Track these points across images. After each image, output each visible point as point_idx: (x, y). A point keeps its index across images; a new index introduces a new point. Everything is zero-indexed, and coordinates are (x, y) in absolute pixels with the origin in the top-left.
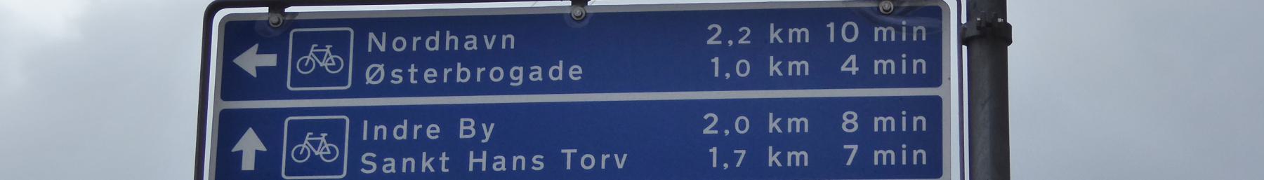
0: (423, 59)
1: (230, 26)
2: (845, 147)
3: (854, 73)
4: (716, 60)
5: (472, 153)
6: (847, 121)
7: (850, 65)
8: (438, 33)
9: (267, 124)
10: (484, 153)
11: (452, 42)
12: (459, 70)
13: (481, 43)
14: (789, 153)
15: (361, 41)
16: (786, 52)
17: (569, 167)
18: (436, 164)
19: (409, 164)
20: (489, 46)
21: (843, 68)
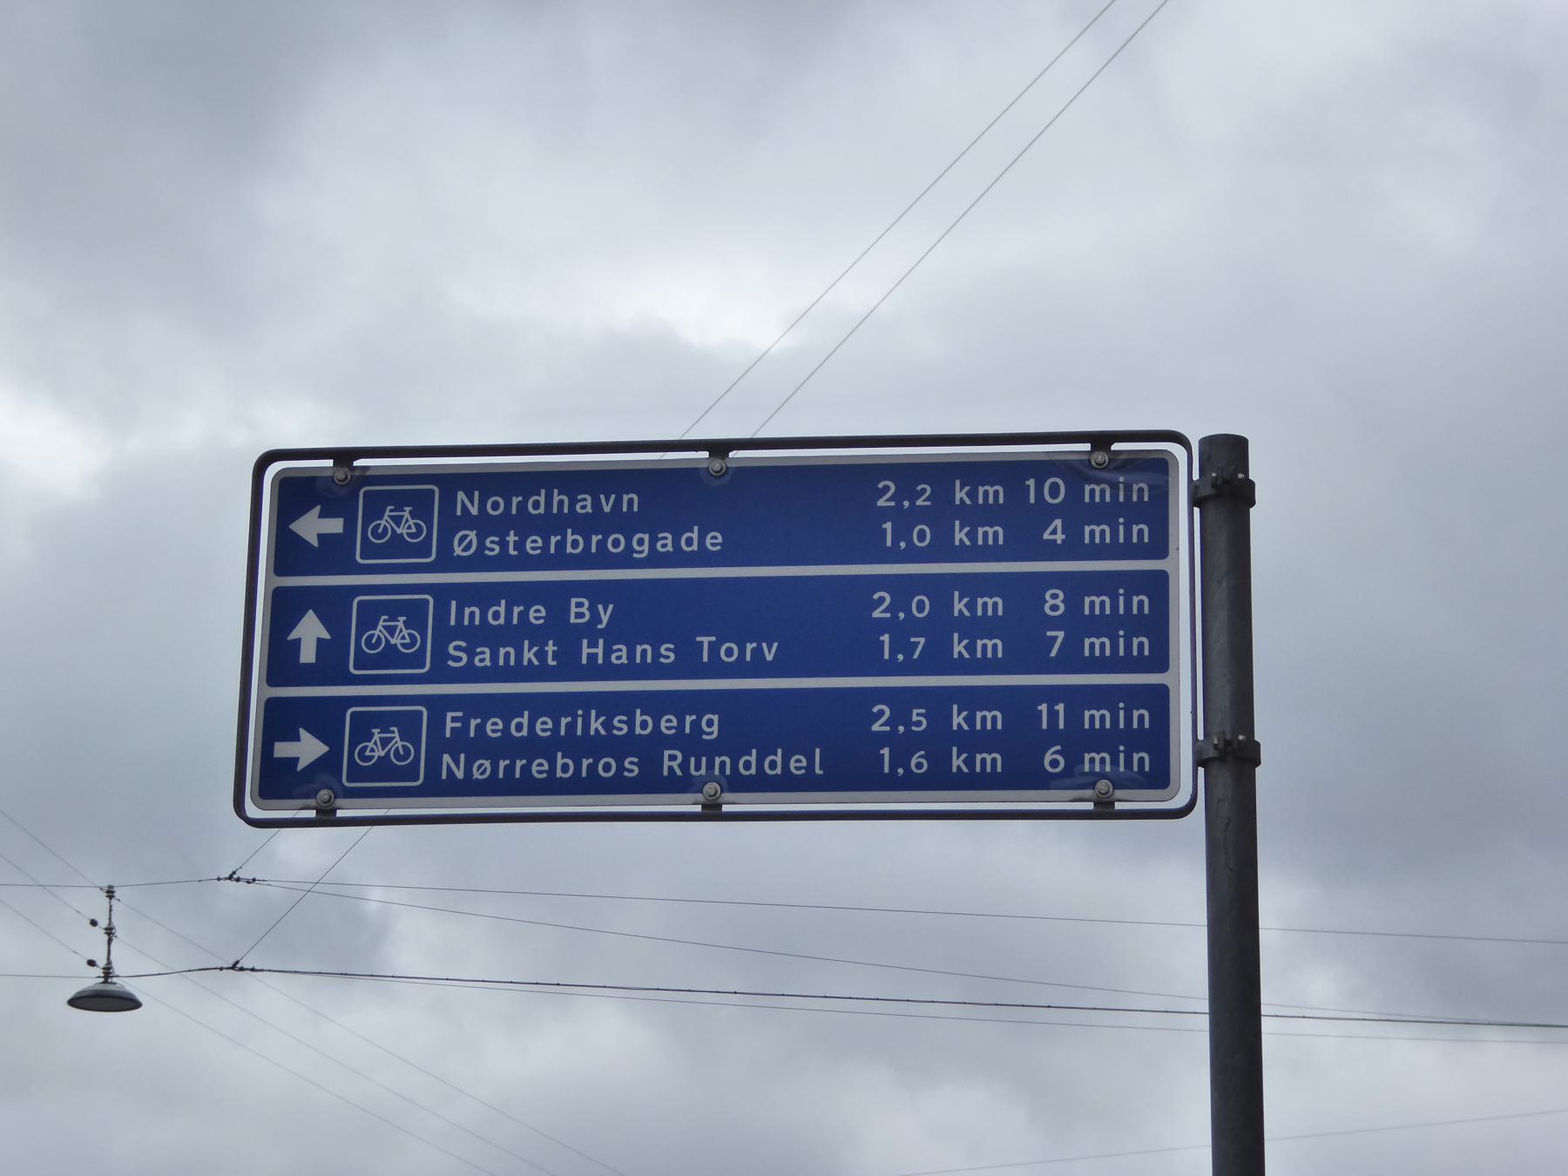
0: (525, 524)
1: (286, 484)
2: (1049, 634)
3: (1059, 542)
5: (585, 642)
6: (1051, 602)
7: (1054, 532)
8: (543, 492)
9: (331, 606)
10: (601, 642)
11: (561, 503)
12: (560, 762)
13: (596, 504)
14: (978, 713)
15: (437, 723)
16: (974, 628)
17: (705, 659)
18: (541, 655)
19: (507, 655)
20: (607, 509)
21: (1046, 536)
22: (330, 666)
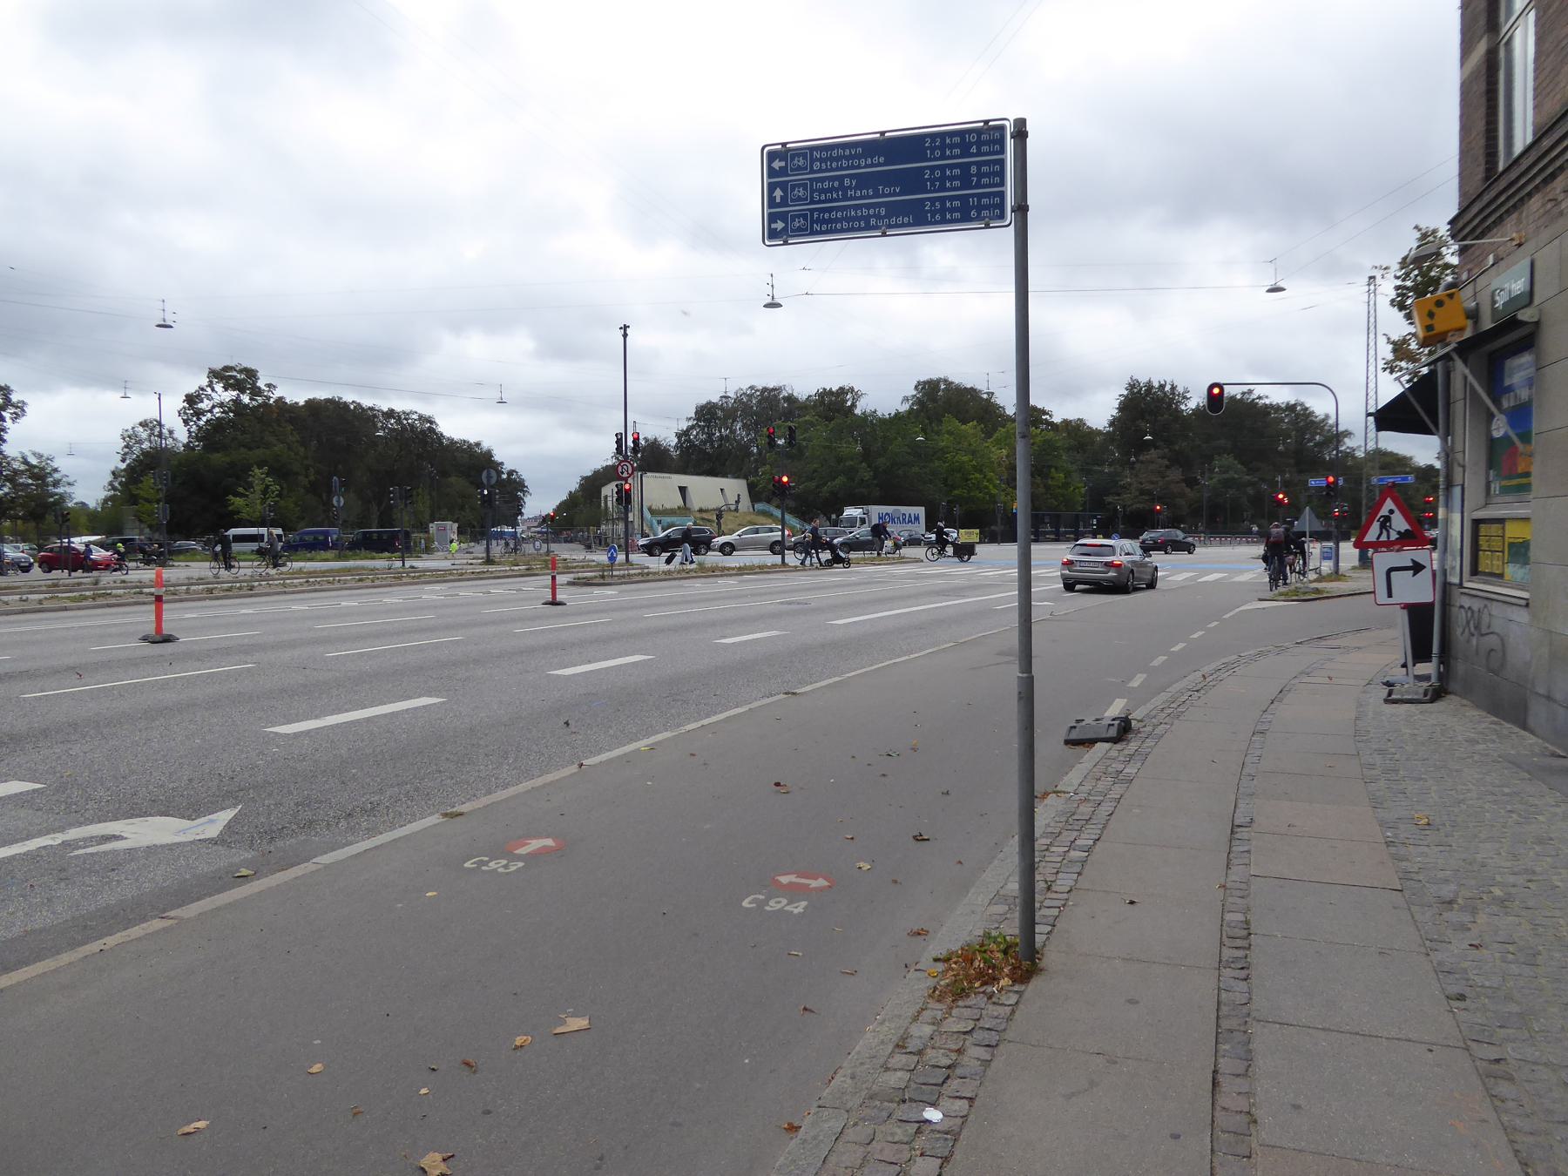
4: (928, 152)
12: (844, 224)
15: (812, 155)
16: (952, 178)
22: (784, 202)
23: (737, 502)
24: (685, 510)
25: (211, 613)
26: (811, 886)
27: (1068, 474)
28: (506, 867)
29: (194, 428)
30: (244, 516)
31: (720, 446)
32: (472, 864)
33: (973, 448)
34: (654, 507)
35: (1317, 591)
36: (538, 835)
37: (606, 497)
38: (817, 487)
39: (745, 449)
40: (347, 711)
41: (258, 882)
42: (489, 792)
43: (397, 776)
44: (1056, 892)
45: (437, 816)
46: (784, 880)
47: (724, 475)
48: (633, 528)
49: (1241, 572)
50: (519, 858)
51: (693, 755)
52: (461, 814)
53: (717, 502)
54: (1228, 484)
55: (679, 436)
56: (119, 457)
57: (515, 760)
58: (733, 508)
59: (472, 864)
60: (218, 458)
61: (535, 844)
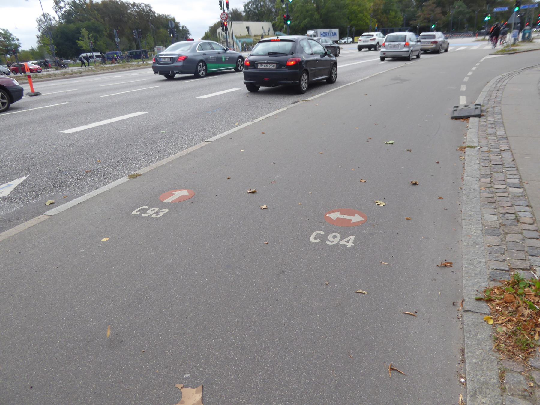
23: (269, 31)
24: (249, 36)
25: (61, 83)
26: (339, 213)
27: (396, 12)
28: (157, 213)
29: (60, 15)
30: (84, 48)
31: (261, 10)
32: (137, 212)
33: (359, 3)
34: (237, 36)
35: (514, 50)
36: (180, 188)
37: (219, 33)
38: (299, 23)
39: (270, 10)
40: (101, 120)
41: (22, 224)
42: (160, 159)
43: (115, 152)
44: (525, 223)
45: (126, 177)
46: (334, 216)
47: (263, 21)
48: (230, 44)
49: (472, 46)
50: (167, 205)
51: (263, 133)
52: (139, 175)
53: (261, 32)
54: (460, 13)
55: (245, 6)
56: (37, 30)
57: (176, 140)
58: (267, 34)
59: (137, 212)
60: (72, 26)
61: (177, 194)
